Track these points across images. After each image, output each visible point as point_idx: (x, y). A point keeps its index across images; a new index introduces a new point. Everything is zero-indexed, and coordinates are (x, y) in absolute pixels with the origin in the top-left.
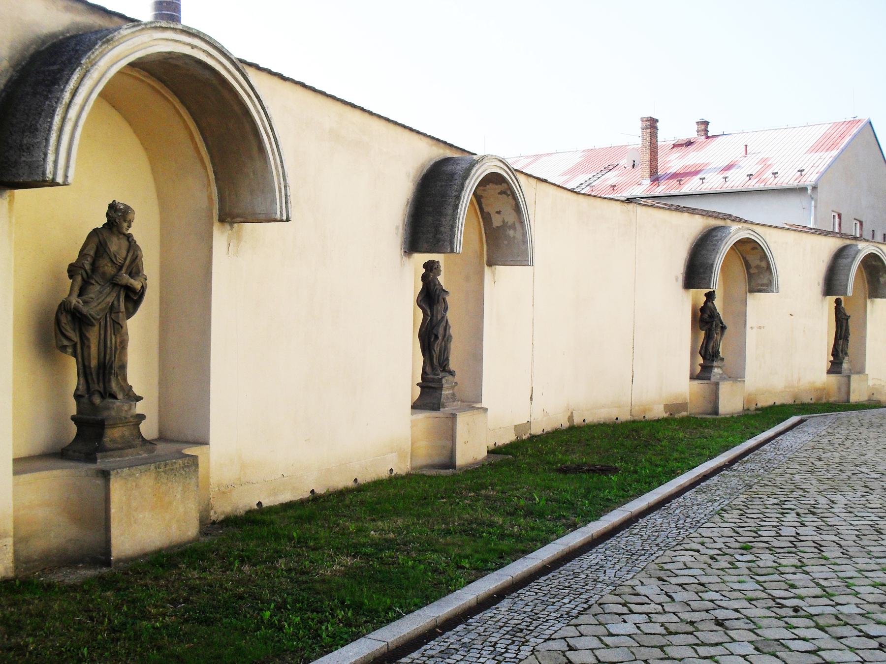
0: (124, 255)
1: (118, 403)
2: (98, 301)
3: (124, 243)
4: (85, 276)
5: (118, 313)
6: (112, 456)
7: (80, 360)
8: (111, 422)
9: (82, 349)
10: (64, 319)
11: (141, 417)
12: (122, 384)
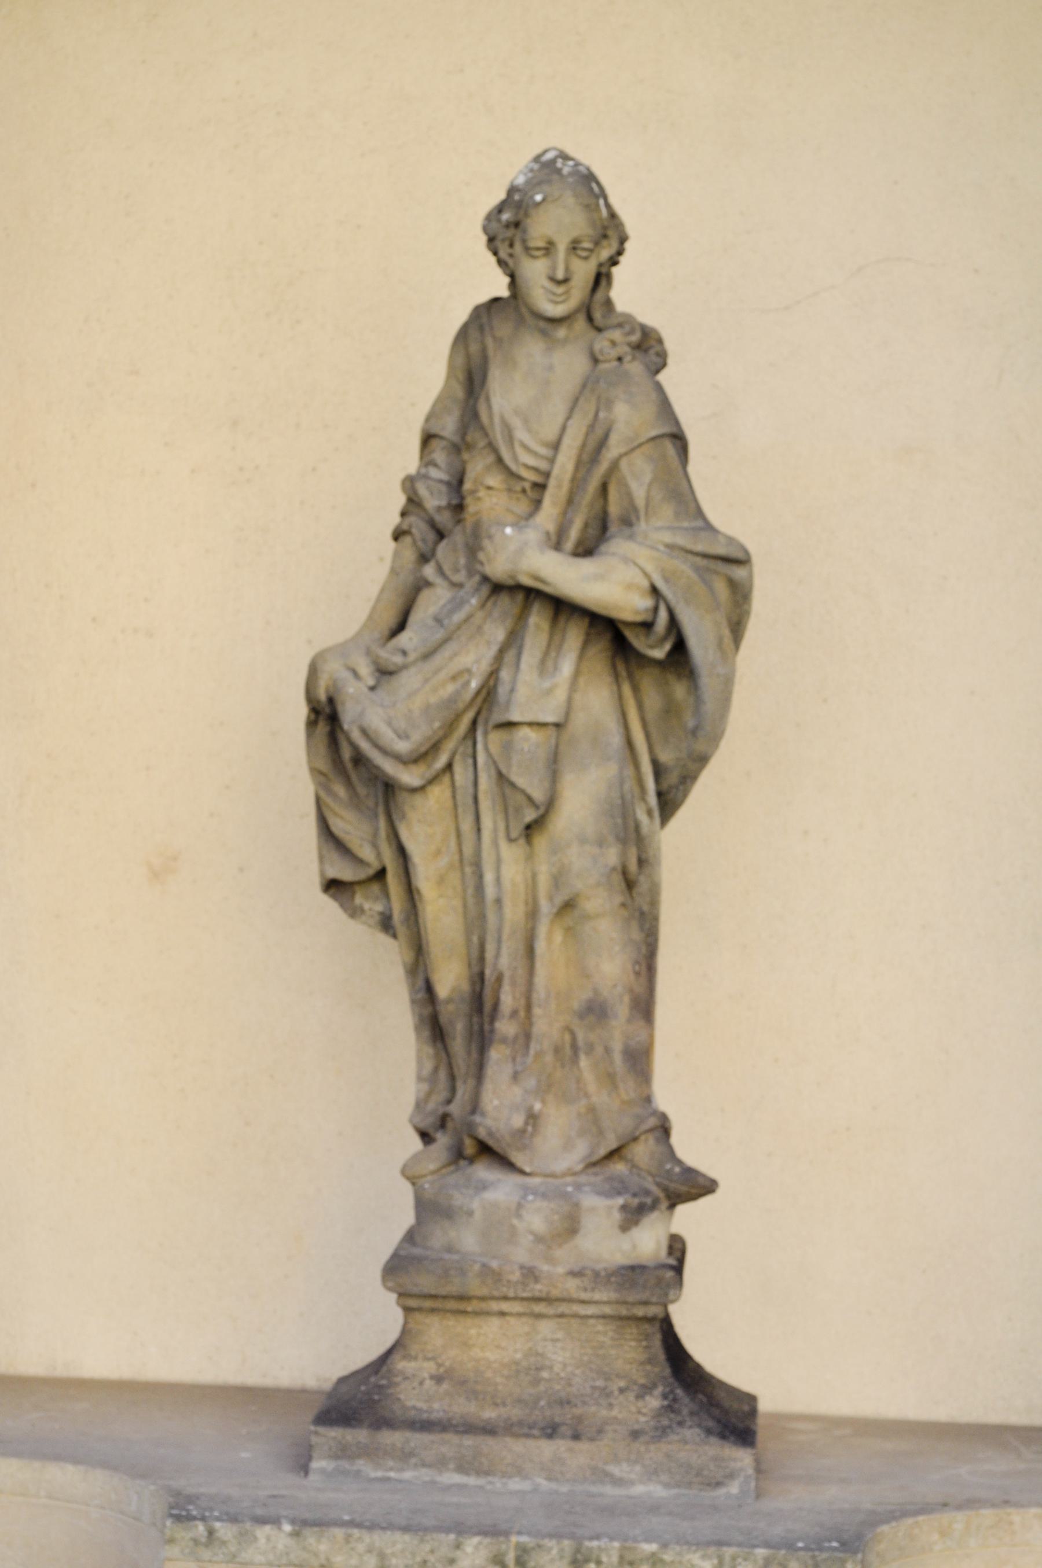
6: (405, 1456)
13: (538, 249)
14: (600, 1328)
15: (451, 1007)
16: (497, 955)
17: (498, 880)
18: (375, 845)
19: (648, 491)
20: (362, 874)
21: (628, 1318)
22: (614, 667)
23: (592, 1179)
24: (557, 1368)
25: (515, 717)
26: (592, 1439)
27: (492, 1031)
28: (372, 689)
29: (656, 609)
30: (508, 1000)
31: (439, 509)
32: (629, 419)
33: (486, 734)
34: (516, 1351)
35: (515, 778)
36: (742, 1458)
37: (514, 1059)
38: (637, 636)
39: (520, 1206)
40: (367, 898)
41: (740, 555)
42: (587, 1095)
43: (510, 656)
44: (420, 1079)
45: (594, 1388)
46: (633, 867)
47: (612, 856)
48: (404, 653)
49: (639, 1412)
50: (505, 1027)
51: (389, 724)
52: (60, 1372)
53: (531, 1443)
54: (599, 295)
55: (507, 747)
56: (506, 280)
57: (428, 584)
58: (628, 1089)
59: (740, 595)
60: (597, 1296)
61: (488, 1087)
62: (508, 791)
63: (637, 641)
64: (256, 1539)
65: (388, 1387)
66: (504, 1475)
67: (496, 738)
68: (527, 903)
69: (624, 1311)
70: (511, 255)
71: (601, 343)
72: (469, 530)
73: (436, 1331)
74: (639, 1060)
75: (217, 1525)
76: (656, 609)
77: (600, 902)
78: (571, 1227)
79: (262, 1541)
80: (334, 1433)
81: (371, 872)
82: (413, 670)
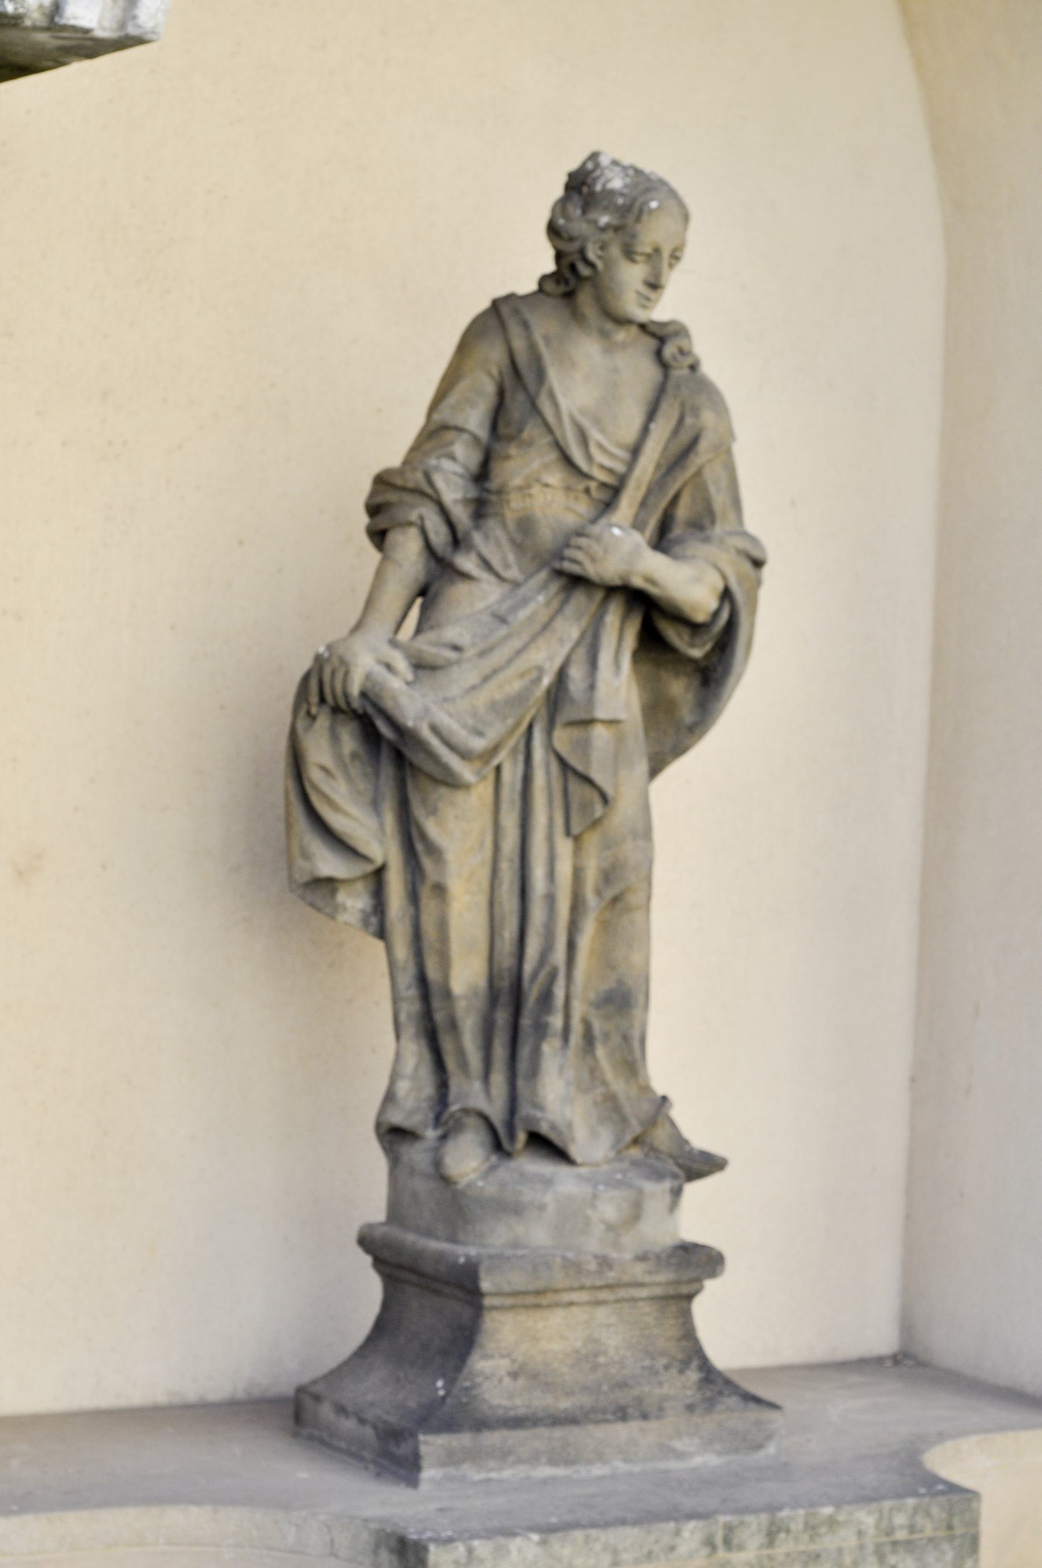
0: (630, 433)
1: (565, 1181)
2: (479, 670)
3: (637, 370)
4: (439, 535)
5: (588, 722)
6: (504, 1455)
7: (402, 951)
8: (518, 1280)
9: (414, 897)
10: (319, 752)
11: (698, 1262)
12: (618, 1085)
24: (611, 1352)
31: (456, 501)
38: (679, 635)
39: (595, 1196)
42: (604, 1083)
45: (643, 1368)
49: (685, 1387)
62: (575, 787)
64: (509, 1552)
66: (589, 1462)
69: (671, 1291)
75: (476, 1543)
76: (716, 614)
79: (514, 1555)
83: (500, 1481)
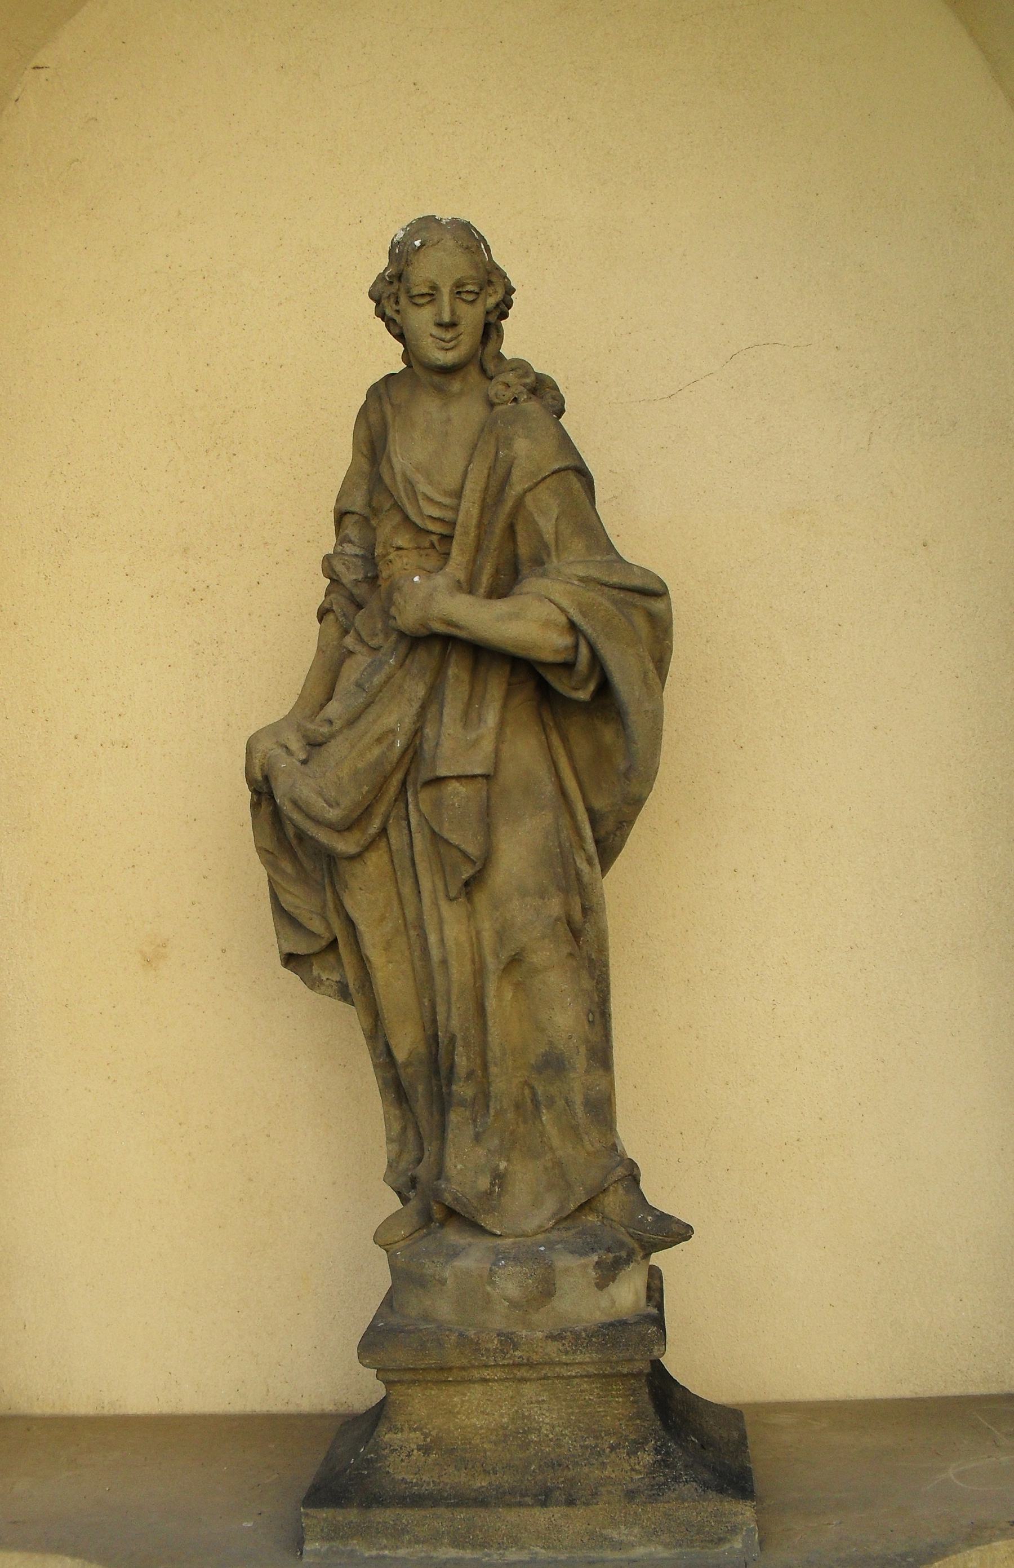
6: (398, 1533)
13: (423, 295)
14: (585, 1386)
15: (410, 1070)
16: (448, 1018)
17: (442, 941)
18: (324, 918)
19: (557, 526)
20: (316, 947)
21: (612, 1375)
22: (540, 715)
23: (565, 1234)
25: (442, 772)
26: (587, 1504)
27: (450, 1094)
28: (304, 762)
29: (576, 647)
30: (462, 1062)
32: (528, 452)
33: (416, 794)
34: (502, 1416)
35: (446, 835)
36: (745, 1512)
37: (475, 1121)
39: (492, 1273)
40: (324, 969)
41: (657, 587)
43: (432, 711)
44: (390, 1140)
46: (577, 915)
47: (555, 906)
48: (330, 722)
49: (633, 1470)
50: (463, 1090)
51: (320, 794)
52: (108, 1411)
53: (524, 1512)
54: (490, 347)
55: (437, 804)
56: (400, 348)
57: (351, 653)
58: (592, 1141)
59: (659, 633)
60: (579, 1358)
61: (450, 1151)
63: (560, 684)
65: (377, 1461)
66: (500, 1546)
67: (426, 796)
68: (473, 962)
69: (608, 1370)
70: (398, 312)
71: (495, 389)
72: (383, 596)
73: (419, 1404)
74: (602, 1109)
77: (545, 953)
78: (546, 1290)
80: (325, 1513)
81: (324, 943)
82: (340, 738)
83: (396, 1559)
